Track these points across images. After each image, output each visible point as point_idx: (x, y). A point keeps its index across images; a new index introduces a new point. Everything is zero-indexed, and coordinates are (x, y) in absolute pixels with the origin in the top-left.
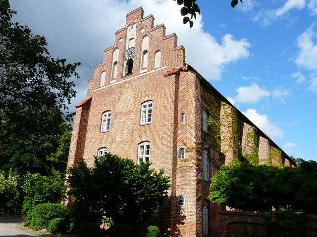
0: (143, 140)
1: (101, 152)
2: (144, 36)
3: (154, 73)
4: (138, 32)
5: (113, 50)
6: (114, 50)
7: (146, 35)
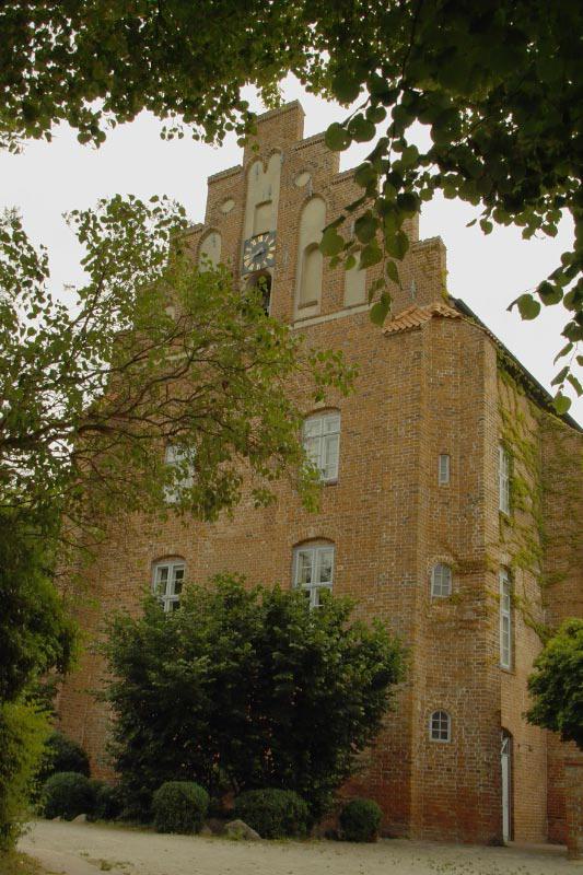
0: (311, 535)
1: (164, 572)
2: (308, 200)
3: (343, 319)
4: (287, 181)
5: (198, 236)
6: (203, 238)
7: (314, 196)
